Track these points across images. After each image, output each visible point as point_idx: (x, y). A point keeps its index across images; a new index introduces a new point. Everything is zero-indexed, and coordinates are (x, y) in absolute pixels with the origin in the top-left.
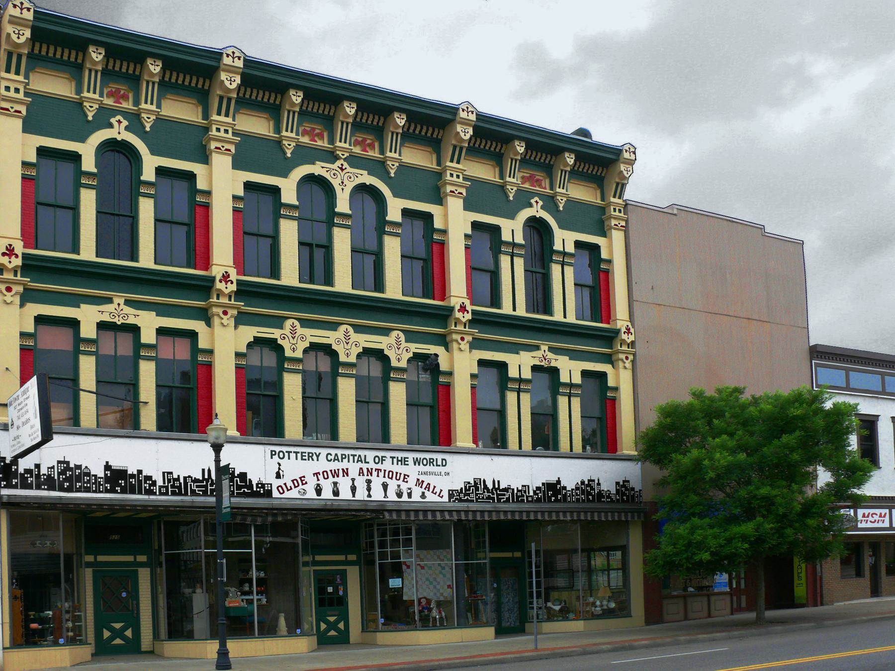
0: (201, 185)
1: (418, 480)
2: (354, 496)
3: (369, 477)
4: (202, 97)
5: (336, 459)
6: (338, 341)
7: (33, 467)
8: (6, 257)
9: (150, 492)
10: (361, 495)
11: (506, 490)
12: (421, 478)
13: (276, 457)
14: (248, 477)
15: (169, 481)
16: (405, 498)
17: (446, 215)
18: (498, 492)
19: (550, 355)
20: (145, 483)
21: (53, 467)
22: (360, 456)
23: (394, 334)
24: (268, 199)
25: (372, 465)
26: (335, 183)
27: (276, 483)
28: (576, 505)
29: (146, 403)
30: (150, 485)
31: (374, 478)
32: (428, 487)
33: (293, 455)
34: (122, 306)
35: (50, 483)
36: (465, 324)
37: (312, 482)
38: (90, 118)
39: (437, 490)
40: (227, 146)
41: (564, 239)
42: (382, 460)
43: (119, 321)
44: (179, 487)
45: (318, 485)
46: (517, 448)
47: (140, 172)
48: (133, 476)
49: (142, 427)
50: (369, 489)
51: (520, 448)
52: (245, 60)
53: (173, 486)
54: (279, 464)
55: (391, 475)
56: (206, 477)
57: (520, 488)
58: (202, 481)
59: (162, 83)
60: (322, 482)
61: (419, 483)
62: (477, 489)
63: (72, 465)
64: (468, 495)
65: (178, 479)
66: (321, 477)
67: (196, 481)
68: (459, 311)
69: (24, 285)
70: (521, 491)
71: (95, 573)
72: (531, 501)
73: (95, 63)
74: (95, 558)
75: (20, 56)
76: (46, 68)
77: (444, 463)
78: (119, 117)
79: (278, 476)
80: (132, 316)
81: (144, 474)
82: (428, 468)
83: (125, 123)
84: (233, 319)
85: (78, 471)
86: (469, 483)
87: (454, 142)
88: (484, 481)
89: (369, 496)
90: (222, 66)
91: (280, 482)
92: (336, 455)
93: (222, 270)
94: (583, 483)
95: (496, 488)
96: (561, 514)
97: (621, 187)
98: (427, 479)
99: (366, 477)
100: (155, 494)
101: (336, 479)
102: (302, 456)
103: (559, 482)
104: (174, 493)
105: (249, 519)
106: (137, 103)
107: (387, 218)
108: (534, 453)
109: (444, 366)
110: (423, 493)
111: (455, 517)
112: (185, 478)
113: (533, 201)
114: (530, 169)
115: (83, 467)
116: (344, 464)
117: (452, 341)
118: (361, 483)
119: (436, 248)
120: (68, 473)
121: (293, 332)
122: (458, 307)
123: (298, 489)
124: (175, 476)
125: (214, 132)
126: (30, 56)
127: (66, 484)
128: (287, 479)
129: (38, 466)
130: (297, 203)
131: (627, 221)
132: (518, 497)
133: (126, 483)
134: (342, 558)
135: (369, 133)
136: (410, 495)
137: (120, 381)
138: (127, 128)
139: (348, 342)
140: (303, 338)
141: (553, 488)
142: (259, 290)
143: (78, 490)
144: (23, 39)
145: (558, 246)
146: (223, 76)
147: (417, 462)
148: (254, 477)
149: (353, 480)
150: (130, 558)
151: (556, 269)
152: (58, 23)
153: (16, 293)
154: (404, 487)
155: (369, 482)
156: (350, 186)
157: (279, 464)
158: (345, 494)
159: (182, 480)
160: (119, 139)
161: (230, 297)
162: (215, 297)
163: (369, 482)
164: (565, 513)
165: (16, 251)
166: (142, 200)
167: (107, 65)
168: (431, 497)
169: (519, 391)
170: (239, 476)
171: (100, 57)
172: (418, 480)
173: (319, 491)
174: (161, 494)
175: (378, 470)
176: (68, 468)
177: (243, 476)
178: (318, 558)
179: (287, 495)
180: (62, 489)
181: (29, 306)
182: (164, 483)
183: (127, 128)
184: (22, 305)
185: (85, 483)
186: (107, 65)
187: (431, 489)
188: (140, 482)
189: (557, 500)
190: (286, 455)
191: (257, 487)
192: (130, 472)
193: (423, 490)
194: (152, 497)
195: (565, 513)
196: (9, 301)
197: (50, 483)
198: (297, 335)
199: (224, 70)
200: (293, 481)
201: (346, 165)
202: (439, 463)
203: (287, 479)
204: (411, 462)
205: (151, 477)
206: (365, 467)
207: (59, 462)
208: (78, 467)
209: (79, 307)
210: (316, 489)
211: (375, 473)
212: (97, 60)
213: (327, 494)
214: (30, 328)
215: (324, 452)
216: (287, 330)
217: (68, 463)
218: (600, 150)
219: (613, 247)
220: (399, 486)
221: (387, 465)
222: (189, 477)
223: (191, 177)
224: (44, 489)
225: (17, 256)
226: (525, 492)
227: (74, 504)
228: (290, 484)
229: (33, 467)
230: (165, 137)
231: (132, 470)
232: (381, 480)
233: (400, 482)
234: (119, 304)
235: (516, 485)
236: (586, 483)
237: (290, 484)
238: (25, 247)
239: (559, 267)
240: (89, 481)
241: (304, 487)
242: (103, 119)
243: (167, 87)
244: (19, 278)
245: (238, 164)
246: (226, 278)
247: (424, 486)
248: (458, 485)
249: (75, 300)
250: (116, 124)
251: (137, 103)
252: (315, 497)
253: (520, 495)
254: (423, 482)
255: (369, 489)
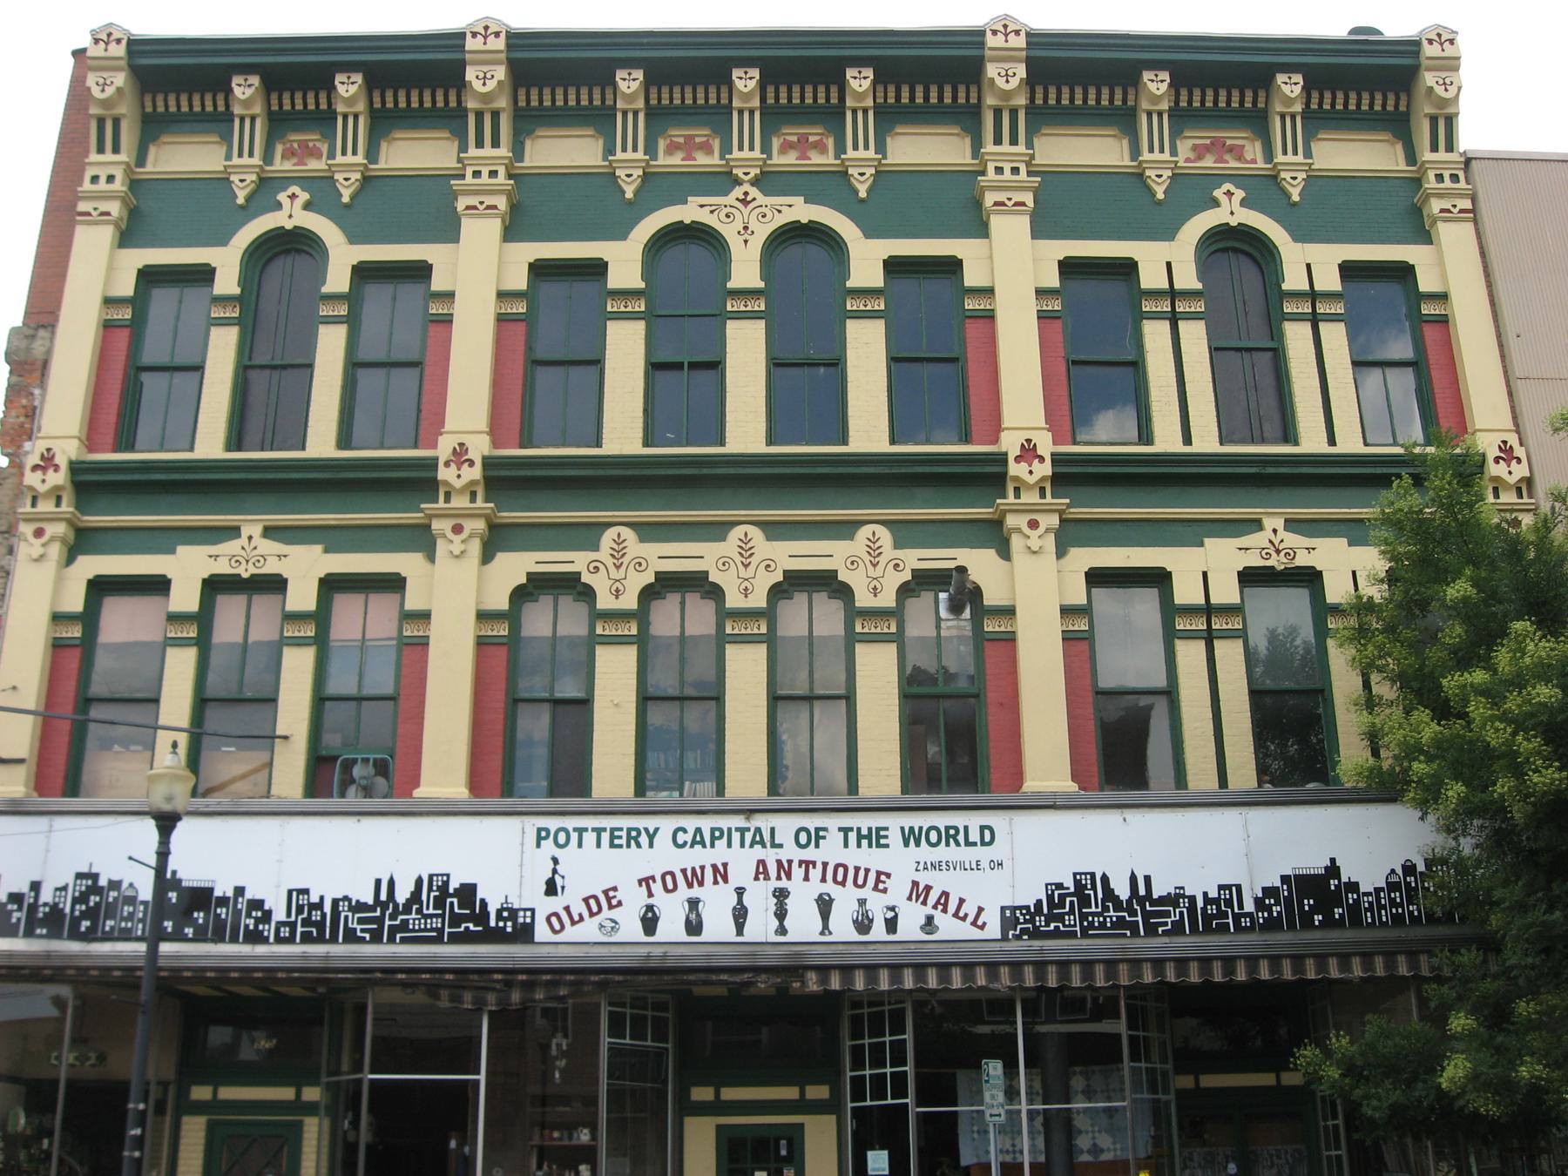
0: (1426, 283)
1: (915, 884)
2: (740, 932)
3: (784, 883)
4: (967, 118)
5: (698, 840)
6: (725, 563)
7: (25, 888)
8: (39, 473)
9: (255, 937)
10: (761, 927)
11: (1172, 900)
12: (924, 879)
13: (548, 844)
14: (479, 896)
15: (300, 909)
16: (878, 932)
17: (1441, 264)
18: (1147, 907)
19: (1292, 540)
20: (249, 915)
21: (65, 888)
22: (758, 830)
23: (865, 532)
24: (1392, 290)
25: (790, 852)
26: (729, 232)
27: (545, 906)
28: (1393, 934)
29: (286, 738)
30: (258, 921)
31: (795, 885)
32: (943, 901)
33: (590, 838)
34: (1282, 533)
35: (54, 921)
36: (1042, 490)
37: (634, 901)
38: (1296, 198)
39: (969, 909)
40: (1018, 197)
41: (1310, 263)
42: (818, 836)
43: (245, 572)
44: (320, 925)
45: (650, 908)
46: (1212, 783)
47: (1279, 277)
48: (223, 901)
49: (1190, 785)
50: (781, 914)
51: (1223, 782)
52: (1028, 35)
53: (306, 922)
54: (555, 861)
55: (841, 874)
56: (383, 897)
57: (1213, 894)
58: (372, 909)
59: (1307, 114)
60: (661, 900)
61: (919, 892)
62: (1084, 901)
63: (103, 882)
64: (1060, 918)
65: (319, 906)
66: (657, 887)
67: (360, 907)
68: (1018, 459)
69: (1061, 512)
70: (1216, 901)
71: (211, 1128)
72: (1251, 929)
73: (1289, 101)
74: (717, 1094)
75: (1014, 112)
76: (1337, 129)
77: (988, 837)
78: (1227, 186)
79: (551, 889)
80: (272, 557)
81: (249, 895)
82: (943, 853)
83: (1239, 194)
84: (1051, 537)
85: (113, 894)
86: (1060, 886)
87: (1428, 110)
88: (1105, 879)
89: (782, 930)
90: (1424, 63)
91: (555, 904)
92: (698, 830)
93: (1496, 439)
94: (1409, 869)
95: (1142, 894)
96: (1333, 963)
97: (1445, 125)
98: (939, 882)
99: (774, 884)
100: (265, 940)
101: (696, 892)
102: (612, 837)
103: (1333, 870)
104: (307, 938)
105: (468, 997)
106: (840, 149)
107: (1285, 287)
108: (778, 801)
109: (993, 596)
110: (930, 919)
111: (1030, 981)
112: (335, 902)
113: (1218, 193)
114: (1208, 128)
115: (125, 885)
116: (718, 854)
117: (1011, 531)
118: (760, 901)
119: (1430, 332)
120: (94, 899)
121: (619, 553)
122: (1013, 452)
123: (597, 919)
124: (315, 899)
125: (1431, 183)
126: (1031, 109)
127: (85, 924)
128: (572, 897)
129: (36, 886)
130: (1199, 286)
131: (1474, 199)
132: (1207, 918)
133: (206, 919)
134: (791, 1093)
135: (812, 123)
136: (891, 925)
137: (249, 694)
138: (1243, 203)
139: (746, 559)
140: (639, 565)
141: (1317, 892)
142: (529, 473)
143: (108, 937)
144: (1014, 83)
145: (1294, 280)
146: (992, 70)
147: (911, 837)
148: (493, 896)
149: (740, 892)
150: (286, 1093)
151: (1297, 337)
152: (571, 45)
153: (1048, 530)
154: (877, 907)
155: (781, 895)
156: (762, 232)
157: (555, 861)
158: (718, 926)
159: (328, 908)
160: (1234, 223)
161: (1042, 491)
162: (29, 502)
163: (781, 895)
164: (1345, 960)
165: (57, 461)
166: (613, 328)
167: (1177, 102)
168: (949, 928)
169: (1209, 638)
170: (457, 892)
171: (1164, 87)
172: (915, 884)
173: (650, 922)
174: (279, 940)
175: (807, 864)
176: (95, 889)
177: (467, 892)
178: (730, 1094)
179: (571, 933)
180: (75, 935)
181: (502, 558)
182: (289, 915)
183: (1243, 203)
184: (1061, 553)
185: (123, 919)
186: (1177, 102)
187: (952, 907)
188: (237, 913)
189: (1329, 923)
190: (574, 836)
191: (499, 916)
192: (218, 893)
193: (928, 910)
194: (261, 949)
195: (1345, 960)
196: (1035, 548)
197: (54, 921)
198: (626, 560)
199: (1429, 69)
200: (586, 900)
201: (754, 192)
202: (974, 836)
203: (572, 897)
204: (895, 838)
205: (261, 902)
206: (771, 856)
207: (79, 876)
208: (115, 885)
209: (1202, 544)
210: (644, 919)
211: (798, 873)
212: (1158, 93)
213: (671, 928)
214: (1078, 595)
215: (667, 825)
216: (604, 554)
217: (95, 877)
218: (215, 52)
219: (1447, 263)
220: (862, 902)
221: (831, 850)
222: (346, 898)
223: (1404, 272)
224: (41, 936)
225: (471, 463)
226: (1229, 903)
227: (78, 968)
228: (578, 908)
229: (25, 888)
230: (896, 201)
231: (223, 889)
232: (815, 887)
233: (867, 892)
234: (1275, 531)
235: (1202, 884)
236: (1421, 867)
237: (578, 908)
238: (1055, 443)
239: (1306, 328)
240: (131, 916)
241: (614, 914)
242: (1193, 191)
243: (1317, 120)
244: (1049, 499)
245: (1040, 230)
246: (1029, 452)
247: (932, 900)
248: (1031, 893)
249: (165, 539)
250: (1223, 199)
251: (840, 149)
252: (855, 936)
253: (1217, 912)
254: (928, 888)
255: (781, 914)
